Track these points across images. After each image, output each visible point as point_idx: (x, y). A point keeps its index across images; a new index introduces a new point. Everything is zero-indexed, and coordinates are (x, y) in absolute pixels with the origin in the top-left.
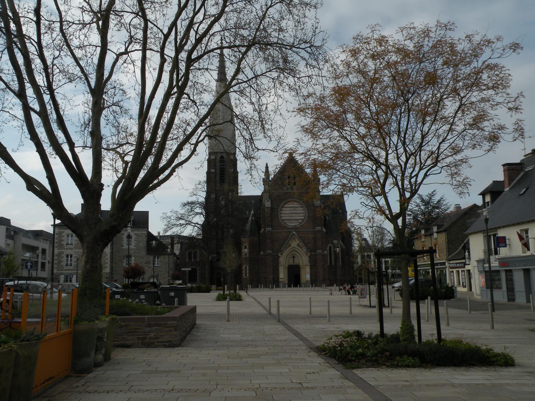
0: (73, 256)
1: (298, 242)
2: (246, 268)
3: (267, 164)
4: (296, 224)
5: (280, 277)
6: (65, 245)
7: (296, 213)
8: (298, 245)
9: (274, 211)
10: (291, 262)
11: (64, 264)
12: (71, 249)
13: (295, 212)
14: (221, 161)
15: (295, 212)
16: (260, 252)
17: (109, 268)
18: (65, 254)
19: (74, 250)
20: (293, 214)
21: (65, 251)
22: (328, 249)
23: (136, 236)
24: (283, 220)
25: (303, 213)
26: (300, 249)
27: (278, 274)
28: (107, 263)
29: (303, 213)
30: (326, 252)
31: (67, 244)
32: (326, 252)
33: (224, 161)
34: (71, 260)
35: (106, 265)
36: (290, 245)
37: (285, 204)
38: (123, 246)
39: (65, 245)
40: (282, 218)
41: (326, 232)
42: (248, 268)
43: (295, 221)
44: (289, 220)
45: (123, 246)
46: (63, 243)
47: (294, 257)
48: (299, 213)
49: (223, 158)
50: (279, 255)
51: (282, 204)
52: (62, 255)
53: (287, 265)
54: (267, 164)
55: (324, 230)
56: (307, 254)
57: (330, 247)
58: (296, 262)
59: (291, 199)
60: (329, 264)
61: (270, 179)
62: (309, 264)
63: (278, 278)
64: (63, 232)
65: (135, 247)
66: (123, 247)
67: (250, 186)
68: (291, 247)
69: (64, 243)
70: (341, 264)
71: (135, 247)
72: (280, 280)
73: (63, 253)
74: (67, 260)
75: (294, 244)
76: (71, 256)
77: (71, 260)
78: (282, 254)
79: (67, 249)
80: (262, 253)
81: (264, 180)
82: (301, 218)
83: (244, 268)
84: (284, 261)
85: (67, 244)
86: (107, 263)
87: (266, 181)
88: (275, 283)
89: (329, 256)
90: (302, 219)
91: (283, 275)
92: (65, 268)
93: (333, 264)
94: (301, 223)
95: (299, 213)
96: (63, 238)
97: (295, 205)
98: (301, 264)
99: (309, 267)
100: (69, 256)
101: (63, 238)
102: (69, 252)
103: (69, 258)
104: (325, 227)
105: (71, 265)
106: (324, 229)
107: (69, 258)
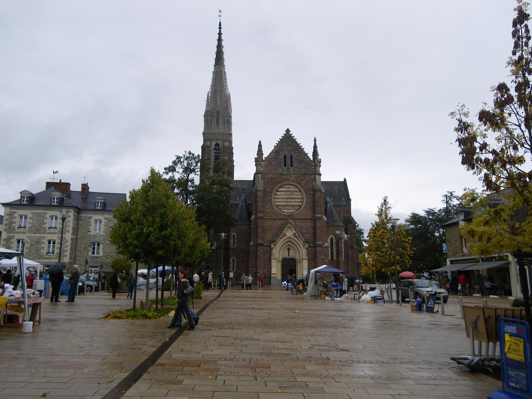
0: (56, 243)
1: (294, 232)
2: (234, 260)
3: (260, 142)
4: (292, 211)
5: (273, 272)
6: (16, 228)
7: (292, 199)
8: (294, 235)
9: (268, 193)
10: (286, 255)
11: (45, 251)
12: (23, 233)
13: (292, 196)
14: (215, 149)
15: (292, 196)
16: (250, 242)
17: (68, 256)
18: (46, 239)
19: (27, 234)
20: (288, 199)
21: (16, 235)
22: (329, 241)
23: (106, 221)
24: (277, 206)
25: (300, 198)
26: (296, 239)
27: (270, 268)
28: (66, 251)
29: (300, 198)
30: (326, 244)
31: (19, 227)
32: (326, 244)
33: (219, 149)
34: (54, 247)
35: (65, 254)
36: (285, 235)
37: (281, 187)
38: (90, 232)
39: (16, 228)
40: (276, 204)
41: (328, 222)
42: (235, 260)
43: (291, 208)
44: (284, 206)
45: (90, 232)
46: (13, 225)
47: (289, 249)
48: (296, 198)
49: (219, 145)
50: (272, 246)
51: (276, 188)
52: (12, 240)
53: (281, 258)
54: (260, 142)
55: (325, 219)
56: (304, 246)
57: (332, 239)
58: (292, 254)
59: (288, 183)
60: (330, 258)
61: (264, 159)
62: (307, 258)
63: (270, 274)
64: (15, 213)
65: (104, 234)
66: (89, 233)
67: (244, 170)
68: (285, 237)
69: (16, 225)
70: (344, 258)
71: (104, 234)
72: (272, 276)
73: (44, 237)
74: (49, 247)
75: (289, 233)
76: (54, 243)
77: (54, 247)
78: (275, 245)
79: (19, 233)
80: (252, 243)
81: (257, 160)
82: (298, 204)
83: (231, 260)
84: (278, 253)
85: (50, 228)
86: (66, 251)
87: (258, 161)
88: (265, 281)
89: (330, 249)
90: (299, 205)
91: (276, 269)
92: (46, 256)
93: (335, 258)
94: (298, 210)
95: (296, 198)
96: (14, 220)
97: (292, 188)
98: (297, 257)
99: (306, 261)
100: (21, 242)
101: (14, 220)
102: (50, 237)
103: (52, 244)
104: (326, 215)
105: (53, 253)
106: (324, 217)
107: (52, 244)
